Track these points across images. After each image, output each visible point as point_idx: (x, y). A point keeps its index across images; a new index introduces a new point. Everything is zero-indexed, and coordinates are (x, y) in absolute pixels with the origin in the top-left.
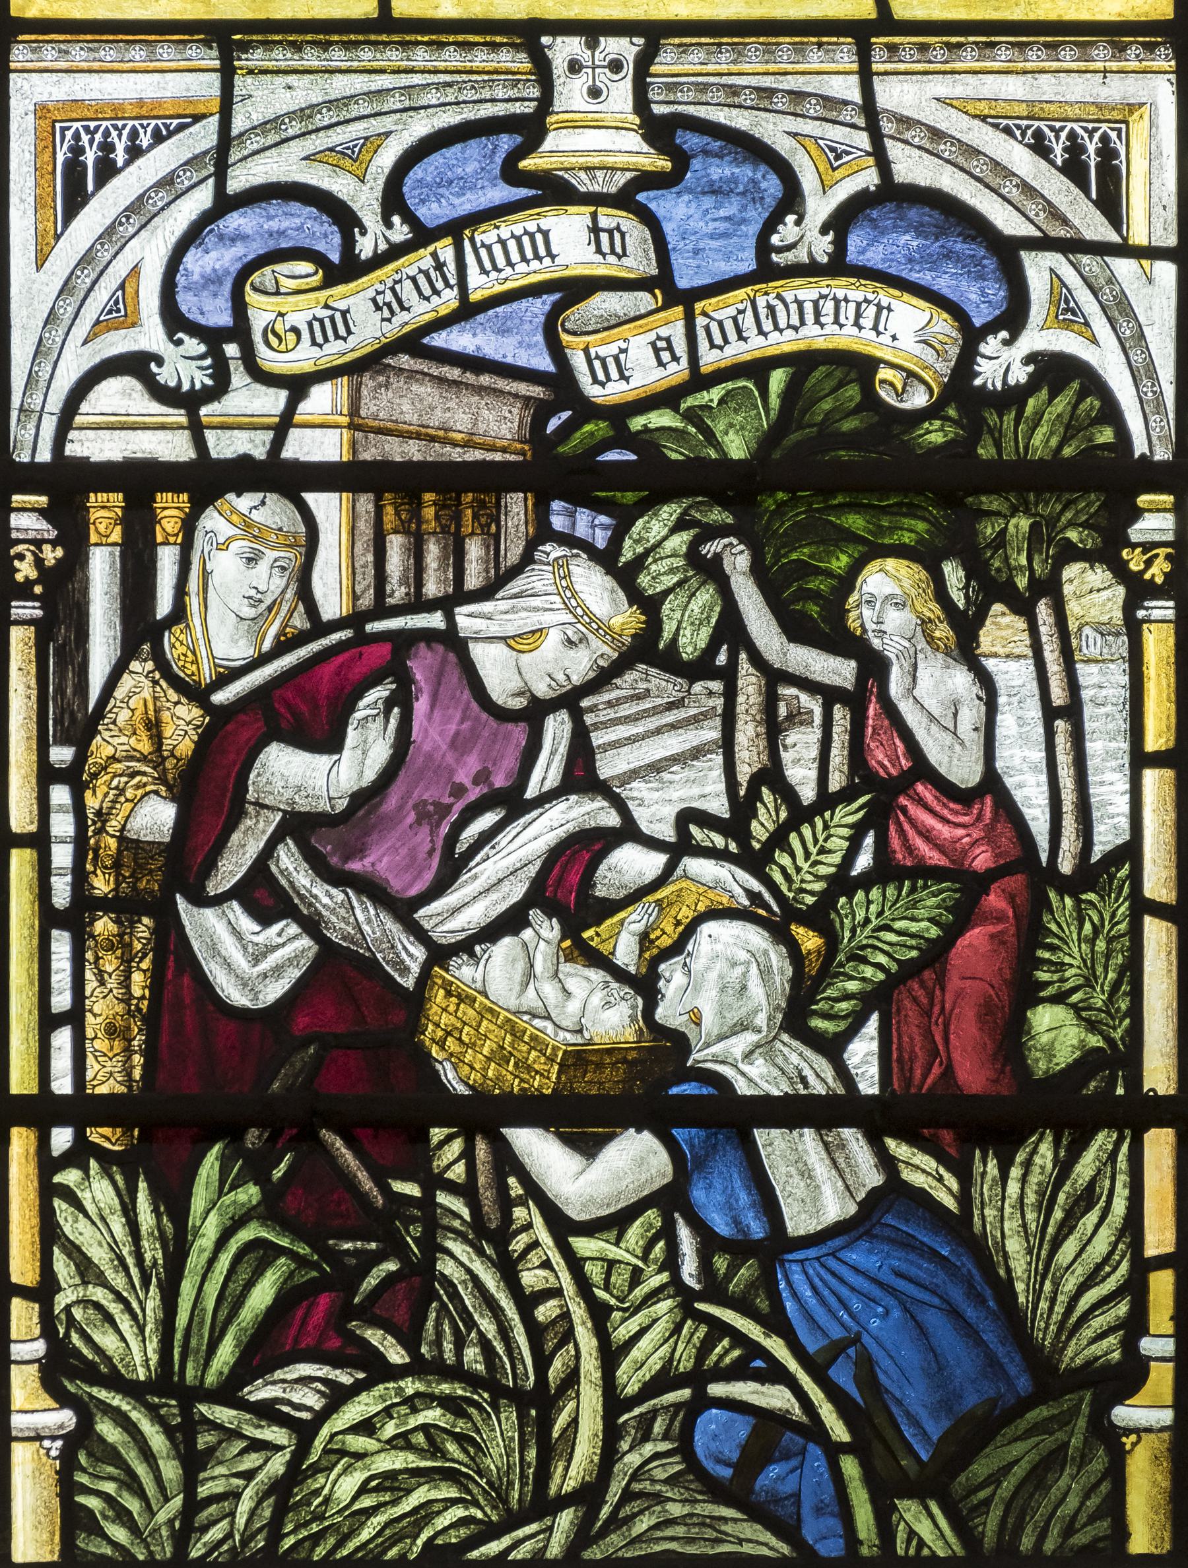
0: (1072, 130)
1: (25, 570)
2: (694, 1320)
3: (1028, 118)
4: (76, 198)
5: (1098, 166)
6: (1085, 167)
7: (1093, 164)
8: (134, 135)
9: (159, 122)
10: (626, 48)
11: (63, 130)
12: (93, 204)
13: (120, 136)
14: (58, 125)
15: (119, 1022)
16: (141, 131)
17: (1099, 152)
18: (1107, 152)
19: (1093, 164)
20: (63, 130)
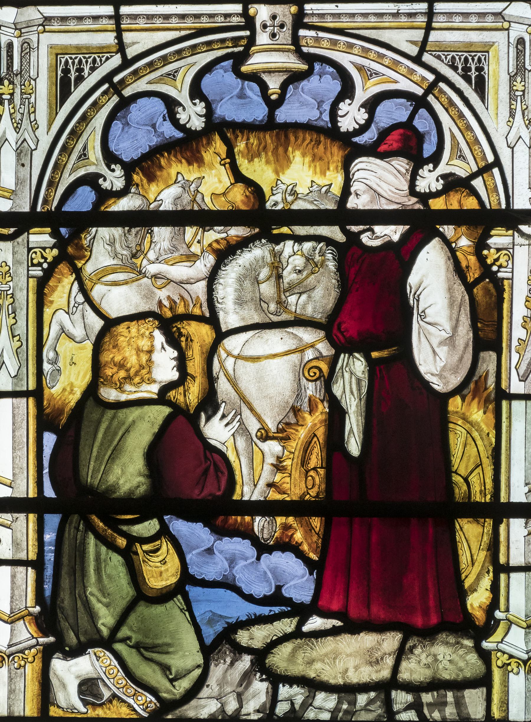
18: (480, 69)
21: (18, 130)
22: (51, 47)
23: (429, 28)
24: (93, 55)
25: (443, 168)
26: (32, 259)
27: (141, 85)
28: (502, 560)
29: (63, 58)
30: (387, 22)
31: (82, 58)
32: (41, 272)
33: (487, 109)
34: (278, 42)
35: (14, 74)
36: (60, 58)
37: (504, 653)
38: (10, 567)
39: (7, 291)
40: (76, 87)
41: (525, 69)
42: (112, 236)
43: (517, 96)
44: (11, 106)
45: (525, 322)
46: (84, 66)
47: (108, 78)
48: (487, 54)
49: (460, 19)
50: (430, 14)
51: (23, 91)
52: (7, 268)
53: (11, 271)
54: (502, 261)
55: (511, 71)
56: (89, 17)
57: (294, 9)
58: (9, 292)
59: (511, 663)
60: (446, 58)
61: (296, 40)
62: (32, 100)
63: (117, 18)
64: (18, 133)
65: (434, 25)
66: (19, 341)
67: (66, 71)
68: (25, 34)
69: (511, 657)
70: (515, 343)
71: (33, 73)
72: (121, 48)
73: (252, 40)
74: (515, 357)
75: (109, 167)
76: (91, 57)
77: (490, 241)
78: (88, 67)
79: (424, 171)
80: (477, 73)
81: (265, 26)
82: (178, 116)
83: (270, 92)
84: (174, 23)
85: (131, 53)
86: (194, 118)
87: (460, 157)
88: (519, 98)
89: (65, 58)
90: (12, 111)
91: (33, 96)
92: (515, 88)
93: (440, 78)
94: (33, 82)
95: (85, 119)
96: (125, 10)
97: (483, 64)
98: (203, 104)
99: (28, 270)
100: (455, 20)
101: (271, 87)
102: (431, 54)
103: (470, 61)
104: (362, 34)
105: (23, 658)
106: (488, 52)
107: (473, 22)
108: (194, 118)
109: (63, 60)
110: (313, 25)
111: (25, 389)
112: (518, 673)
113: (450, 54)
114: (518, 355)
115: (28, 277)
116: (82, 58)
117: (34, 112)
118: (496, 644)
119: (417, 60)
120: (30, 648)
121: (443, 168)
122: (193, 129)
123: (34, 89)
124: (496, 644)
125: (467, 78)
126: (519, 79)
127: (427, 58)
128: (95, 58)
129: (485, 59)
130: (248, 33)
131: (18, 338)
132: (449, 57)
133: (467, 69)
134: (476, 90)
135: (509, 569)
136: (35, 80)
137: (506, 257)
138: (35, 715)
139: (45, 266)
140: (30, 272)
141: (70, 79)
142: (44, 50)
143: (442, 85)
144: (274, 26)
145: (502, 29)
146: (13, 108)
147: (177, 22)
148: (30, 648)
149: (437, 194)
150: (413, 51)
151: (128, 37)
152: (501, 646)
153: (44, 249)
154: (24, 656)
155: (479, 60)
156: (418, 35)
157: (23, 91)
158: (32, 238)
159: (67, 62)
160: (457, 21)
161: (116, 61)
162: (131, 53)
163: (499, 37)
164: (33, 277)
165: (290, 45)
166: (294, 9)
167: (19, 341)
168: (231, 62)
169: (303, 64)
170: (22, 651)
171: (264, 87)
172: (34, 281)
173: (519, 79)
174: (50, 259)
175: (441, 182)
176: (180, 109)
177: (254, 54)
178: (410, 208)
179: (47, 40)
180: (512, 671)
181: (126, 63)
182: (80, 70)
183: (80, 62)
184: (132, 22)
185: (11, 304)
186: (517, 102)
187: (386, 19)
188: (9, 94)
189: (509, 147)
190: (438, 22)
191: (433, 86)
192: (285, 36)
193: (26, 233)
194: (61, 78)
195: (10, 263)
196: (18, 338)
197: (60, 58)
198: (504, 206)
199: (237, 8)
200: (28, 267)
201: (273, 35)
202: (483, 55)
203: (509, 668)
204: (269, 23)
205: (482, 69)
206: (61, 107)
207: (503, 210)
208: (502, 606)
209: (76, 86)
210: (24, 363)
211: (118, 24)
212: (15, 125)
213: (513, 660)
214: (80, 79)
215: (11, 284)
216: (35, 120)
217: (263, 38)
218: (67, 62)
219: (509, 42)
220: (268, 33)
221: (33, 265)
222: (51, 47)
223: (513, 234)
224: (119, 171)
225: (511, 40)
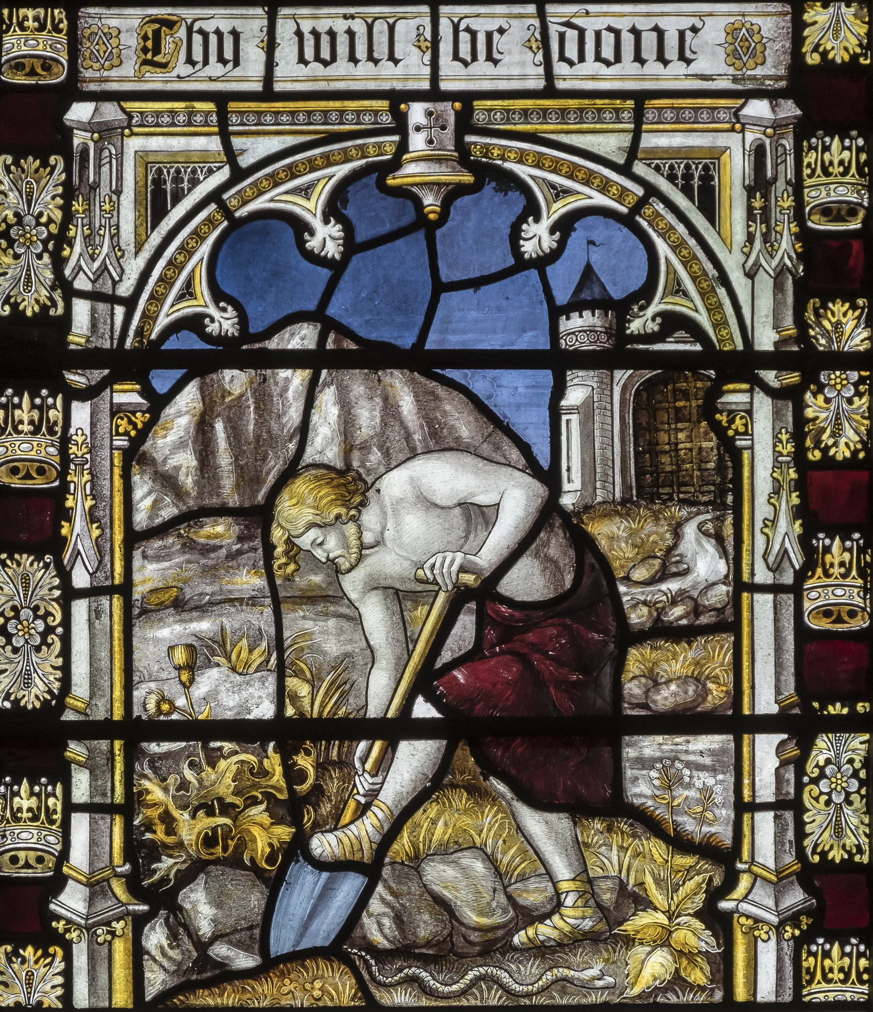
0: (194, 167)
1: (845, 711)
2: (748, 592)
3: (204, 162)
4: (159, 213)
5: (699, 187)
6: (692, 187)
7: (696, 186)
8: (194, 171)
9: (673, 161)
10: (630, 103)
11: (151, 167)
12: (170, 214)
13: (202, 171)
14: (149, 165)
15: (447, 526)
16: (199, 170)
17: (701, 178)
18: (707, 178)
19: (696, 186)
20: (151, 167)
22: (716, 154)
26: (117, 427)
28: (746, 577)
42: (354, 841)
47: (215, 196)
48: (717, 161)
58: (86, 467)
61: (462, 148)
70: (759, 525)
72: (231, 155)
73: (403, 147)
75: (217, 303)
85: (245, 161)
90: (87, 232)
93: (651, 191)
95: (186, 251)
99: (112, 440)
106: (718, 159)
118: (735, 903)
119: (625, 170)
123: (116, 205)
124: (735, 903)
125: (687, 191)
130: (396, 138)
134: (700, 208)
135: (755, 807)
138: (131, 1006)
139: (133, 433)
141: (165, 191)
151: (237, 142)
152: (744, 907)
156: (626, 140)
161: (223, 175)
162: (245, 161)
163: (733, 141)
164: (118, 448)
165: (452, 151)
168: (375, 176)
171: (417, 202)
181: (238, 174)
182: (177, 180)
191: (642, 202)
193: (108, 391)
194: (153, 191)
200: (112, 436)
206: (153, 229)
208: (746, 856)
217: (417, 142)
221: (118, 434)
225: (747, 147)
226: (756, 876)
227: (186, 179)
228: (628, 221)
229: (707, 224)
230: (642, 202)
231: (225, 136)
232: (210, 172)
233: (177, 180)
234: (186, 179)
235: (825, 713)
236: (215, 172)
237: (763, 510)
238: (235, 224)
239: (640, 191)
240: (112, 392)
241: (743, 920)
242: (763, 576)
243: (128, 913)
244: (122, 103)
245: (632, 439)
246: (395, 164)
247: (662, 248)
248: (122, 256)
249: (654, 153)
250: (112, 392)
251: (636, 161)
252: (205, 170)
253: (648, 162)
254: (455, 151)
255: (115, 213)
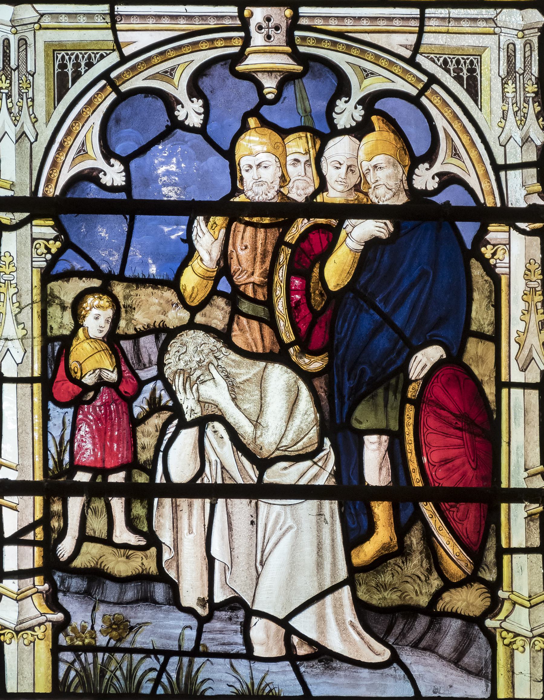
18: (471, 71)
21: (521, 127)
22: (48, 44)
23: (421, 33)
24: (76, 52)
25: (438, 168)
27: (138, 82)
29: (59, 54)
30: (382, 25)
31: (65, 55)
32: (45, 263)
33: (481, 110)
34: (273, 44)
35: (12, 69)
36: (478, 58)
37: (508, 631)
38: (16, 547)
39: (10, 281)
40: (73, 83)
41: (515, 72)
43: (23, 93)
44: (9, 100)
45: (524, 314)
46: (462, 65)
47: (105, 75)
48: (479, 57)
49: (385, 23)
50: (422, 19)
51: (21, 85)
52: (11, 258)
53: (15, 261)
54: (499, 254)
55: (501, 73)
56: (167, 16)
57: (288, 12)
58: (12, 282)
59: (515, 641)
60: (438, 60)
61: (290, 41)
62: (30, 95)
63: (114, 18)
64: (16, 126)
65: (426, 29)
66: (23, 329)
67: (63, 66)
68: (528, 36)
69: (516, 635)
70: (514, 335)
71: (30, 68)
72: (118, 46)
73: (247, 41)
74: (515, 348)
76: (87, 53)
77: (488, 237)
78: (72, 63)
79: (422, 169)
80: (461, 74)
81: (260, 28)
82: (176, 113)
83: (265, 91)
84: (166, 23)
85: (127, 51)
86: (193, 115)
87: (455, 155)
88: (24, 94)
89: (62, 54)
91: (31, 90)
92: (527, 90)
93: (433, 79)
94: (30, 78)
96: (121, 9)
97: (475, 66)
98: (201, 102)
99: (32, 261)
100: (97, 20)
101: (266, 85)
102: (427, 57)
103: (450, 63)
104: (359, 37)
105: (32, 634)
106: (480, 56)
107: (82, 22)
108: (193, 115)
109: (60, 56)
110: (316, 28)
111: (29, 375)
112: (523, 652)
113: (469, 58)
114: (518, 345)
115: (32, 267)
116: (65, 55)
117: (33, 106)
119: (412, 61)
120: (39, 625)
121: (438, 168)
122: (191, 125)
125: (458, 79)
126: (510, 82)
127: (420, 59)
128: (90, 54)
129: (477, 63)
130: (242, 34)
131: (22, 326)
132: (441, 60)
133: (458, 70)
134: (468, 91)
136: (33, 76)
137: (503, 251)
140: (34, 263)
142: (40, 47)
143: (435, 87)
144: (268, 28)
145: (495, 34)
146: (11, 102)
147: (215, 23)
148: (39, 625)
149: (436, 192)
150: (407, 54)
151: (122, 37)
153: (48, 240)
154: (33, 633)
155: (472, 63)
156: (412, 39)
157: (21, 85)
158: (35, 230)
159: (63, 58)
160: (333, 24)
161: (114, 58)
163: (489, 41)
166: (288, 12)
167: (23, 329)
169: (298, 65)
170: (32, 628)
171: (260, 87)
172: (38, 271)
173: (510, 82)
174: (54, 251)
175: (437, 179)
176: (179, 107)
177: (249, 54)
178: (352, 202)
179: (44, 36)
180: (517, 649)
181: (124, 60)
182: (77, 65)
183: (77, 57)
184: (473, 25)
185: (16, 293)
186: (529, 105)
187: (332, 22)
188: (533, 92)
189: (500, 145)
190: (431, 24)
192: (280, 38)
195: (14, 254)
196: (22, 326)
197: (478, 58)
198: (499, 205)
199: (233, 10)
201: (269, 37)
202: (475, 59)
203: (515, 646)
204: (264, 25)
205: (474, 70)
207: (499, 208)
209: (74, 81)
210: (29, 350)
211: (114, 22)
212: (519, 122)
213: (519, 638)
214: (77, 76)
215: (15, 274)
216: (33, 113)
217: (258, 39)
218: (63, 58)
219: (499, 48)
220: (263, 35)
222: (48, 44)
223: (510, 229)
224: (118, 166)
226: (514, 603)
227: (83, 64)
228: (415, 101)
229: (472, 103)
230: (427, 87)
231: (115, 31)
232: (102, 57)
233: (77, 65)
234: (83, 64)
235: (315, 200)
236: (105, 57)
237: (517, 326)
238: (122, 97)
239: (425, 79)
240: (32, 226)
241: (504, 634)
242: (517, 377)
243: (47, 621)
244: (34, 5)
245: (465, 312)
246: (240, 57)
247: (440, 123)
248: (36, 121)
249: (62, 46)
250: (32, 226)
251: (418, 55)
252: (98, 56)
253: (426, 55)
254: (287, 45)
255: (31, 90)
